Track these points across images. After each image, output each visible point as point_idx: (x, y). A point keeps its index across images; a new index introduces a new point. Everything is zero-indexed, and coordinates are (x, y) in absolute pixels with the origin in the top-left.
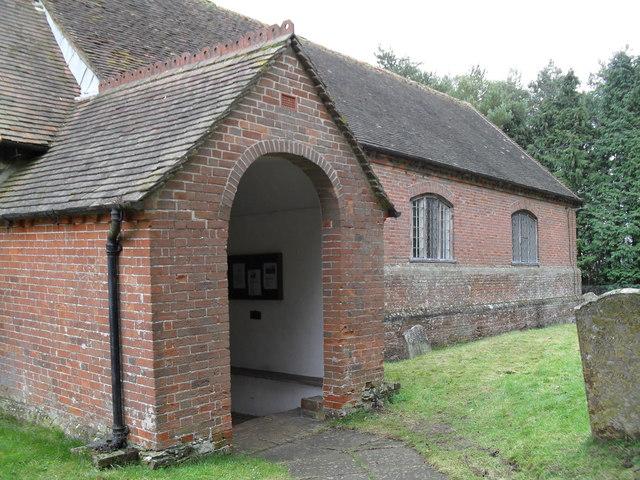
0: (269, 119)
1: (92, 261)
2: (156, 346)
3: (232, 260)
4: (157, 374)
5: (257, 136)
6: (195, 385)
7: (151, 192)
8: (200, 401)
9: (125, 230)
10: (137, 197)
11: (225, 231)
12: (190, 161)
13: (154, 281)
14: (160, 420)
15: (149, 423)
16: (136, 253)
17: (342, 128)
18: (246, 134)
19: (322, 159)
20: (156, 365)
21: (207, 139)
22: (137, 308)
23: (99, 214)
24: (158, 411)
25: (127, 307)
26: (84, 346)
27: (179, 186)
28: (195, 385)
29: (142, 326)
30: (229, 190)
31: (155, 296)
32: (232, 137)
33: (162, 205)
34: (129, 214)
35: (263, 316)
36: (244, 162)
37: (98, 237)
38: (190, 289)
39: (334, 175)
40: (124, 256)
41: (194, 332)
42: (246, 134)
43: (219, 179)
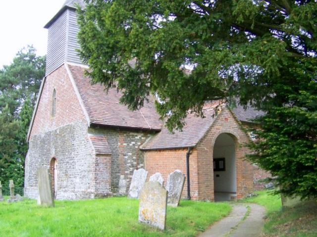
0: (222, 125)
1: (181, 159)
2: (198, 177)
3: (214, 160)
4: (198, 183)
5: (219, 129)
6: (206, 187)
7: (197, 144)
8: (207, 191)
9: (191, 152)
10: (194, 145)
11: (212, 152)
12: (205, 137)
13: (198, 163)
14: (199, 194)
15: (196, 195)
16: (193, 157)
17: (150, 150)
18: (217, 129)
19: (235, 133)
20: (198, 181)
21: (208, 131)
22: (194, 169)
23: (184, 148)
24: (199, 192)
25: (191, 169)
26: (273, 95)
27: (202, 142)
28: (206, 187)
29: (195, 173)
30: (213, 142)
31: (198, 166)
32: (213, 130)
33: (199, 146)
34: (192, 148)
35: (220, 176)
36: (216, 136)
37: (185, 152)
38: (205, 165)
39: (238, 137)
40: (190, 158)
41: (206, 175)
42: (217, 129)
43: (211, 140)
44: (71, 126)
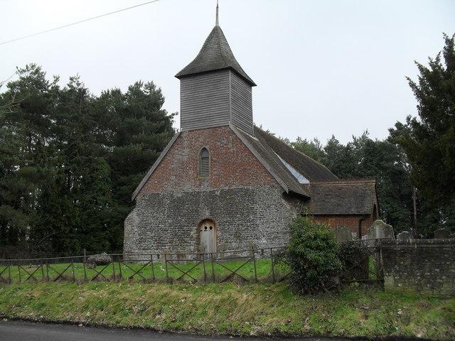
44: (248, 190)
